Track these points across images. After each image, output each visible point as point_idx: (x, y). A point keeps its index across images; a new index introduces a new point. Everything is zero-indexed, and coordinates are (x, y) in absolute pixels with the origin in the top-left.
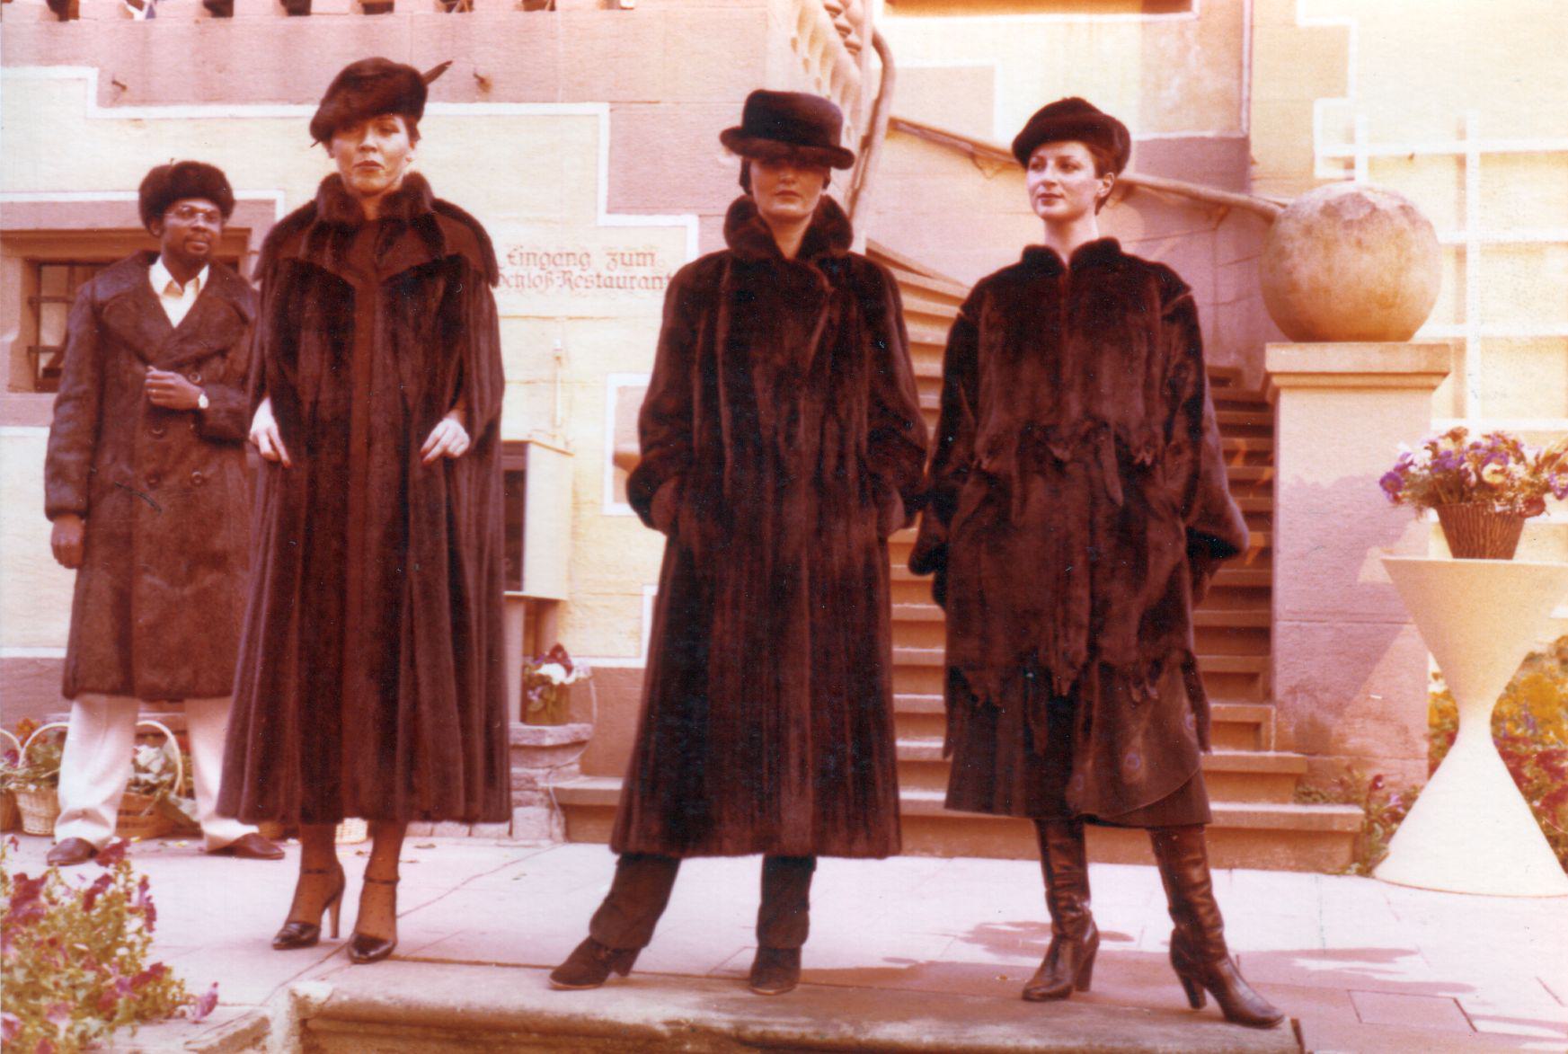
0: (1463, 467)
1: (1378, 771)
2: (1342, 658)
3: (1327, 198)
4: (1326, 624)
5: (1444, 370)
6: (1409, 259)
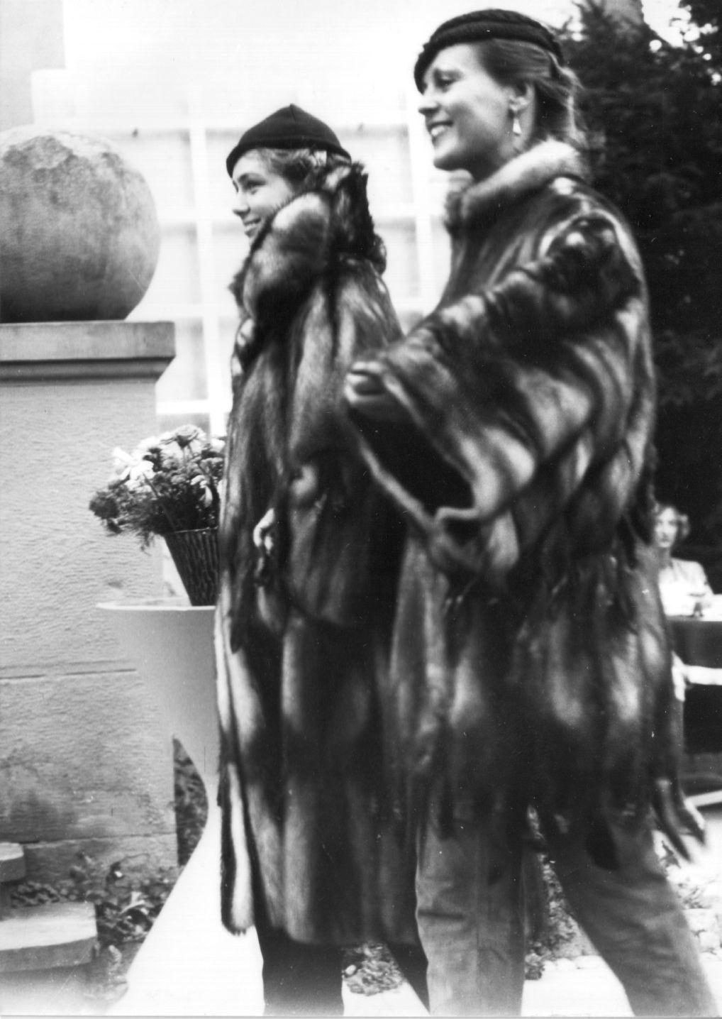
0: (194, 481)
1: (117, 855)
2: (64, 718)
3: (11, 143)
4: (42, 679)
5: (168, 354)
6: (117, 219)
